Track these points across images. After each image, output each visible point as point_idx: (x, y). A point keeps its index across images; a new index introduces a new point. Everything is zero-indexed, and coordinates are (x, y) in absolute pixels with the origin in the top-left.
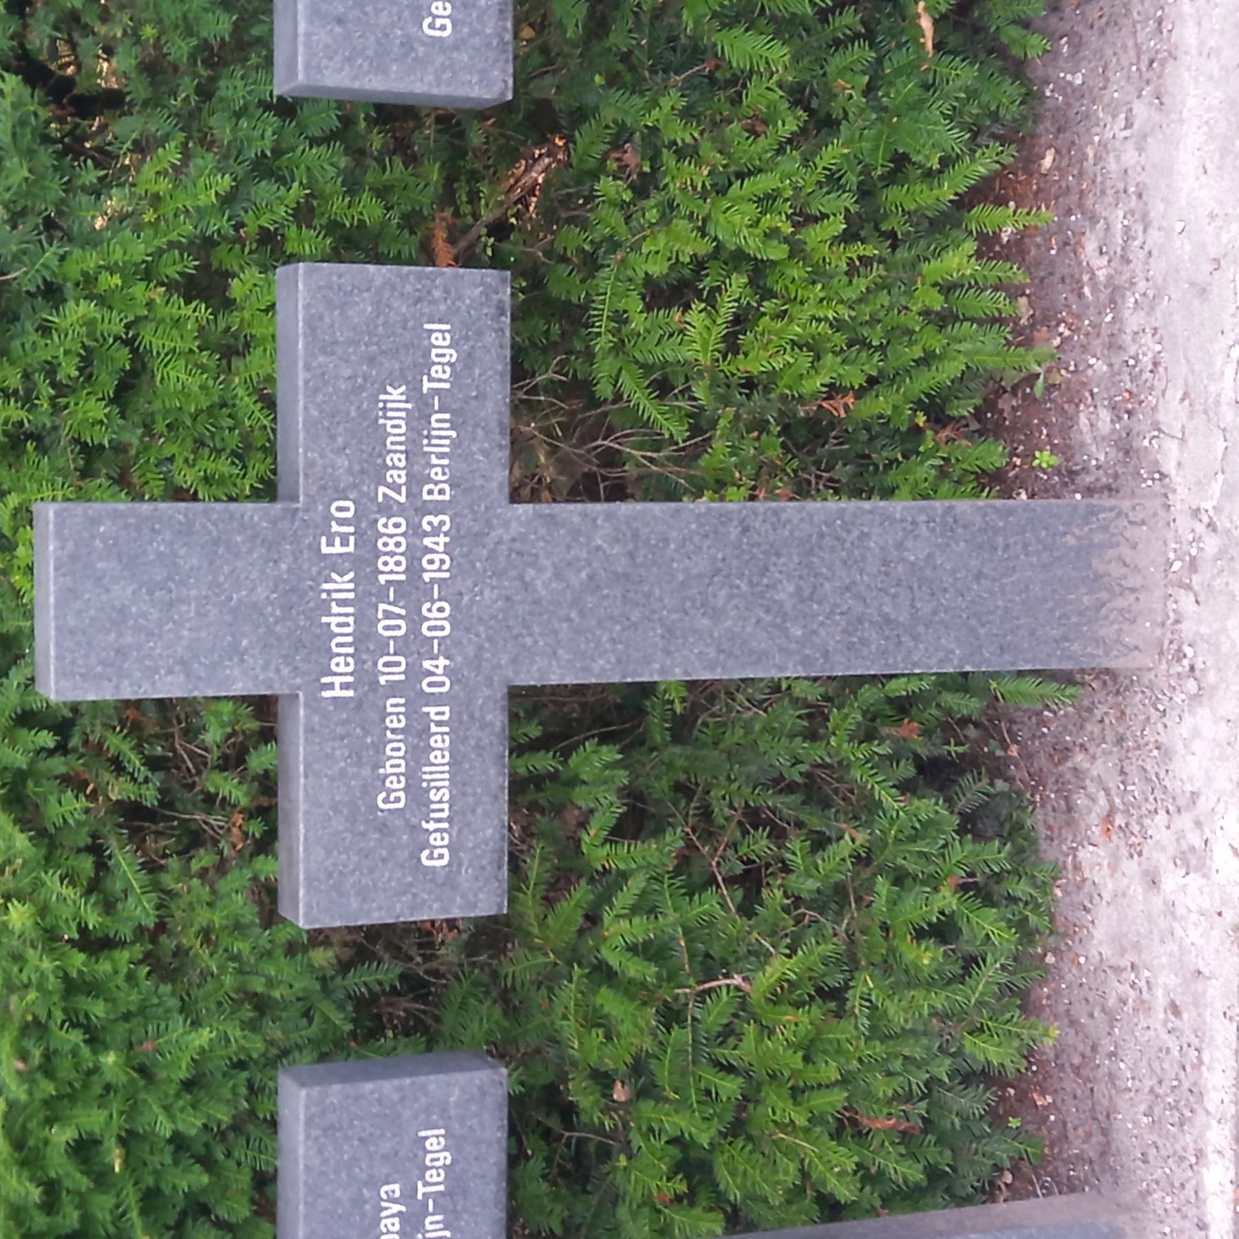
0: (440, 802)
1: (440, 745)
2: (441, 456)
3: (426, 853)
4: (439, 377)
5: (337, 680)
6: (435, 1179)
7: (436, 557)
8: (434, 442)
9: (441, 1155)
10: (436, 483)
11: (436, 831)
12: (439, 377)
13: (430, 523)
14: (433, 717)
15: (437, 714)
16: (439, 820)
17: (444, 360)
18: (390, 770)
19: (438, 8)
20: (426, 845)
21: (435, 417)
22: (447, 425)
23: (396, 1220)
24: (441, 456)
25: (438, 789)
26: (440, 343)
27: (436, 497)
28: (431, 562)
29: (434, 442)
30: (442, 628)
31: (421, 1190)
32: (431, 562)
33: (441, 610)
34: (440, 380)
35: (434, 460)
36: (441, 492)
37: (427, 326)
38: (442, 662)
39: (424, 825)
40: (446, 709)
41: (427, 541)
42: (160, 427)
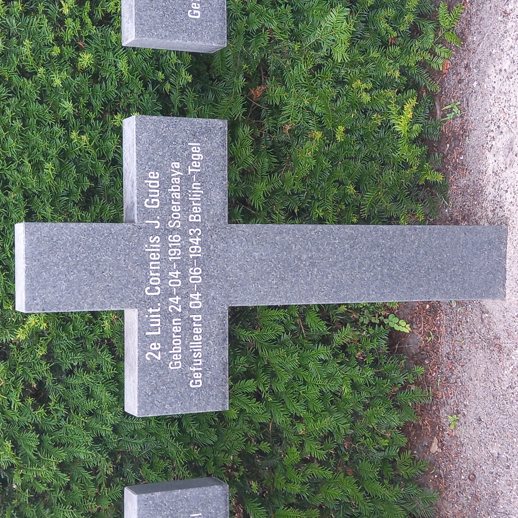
0: (198, 358)
1: (197, 332)
2: (196, 202)
4: (195, 167)
6: (196, 166)
7: (195, 247)
8: (194, 195)
9: (199, 155)
10: (194, 214)
11: (196, 371)
12: (195, 167)
13: (192, 232)
14: (194, 319)
17: (198, 159)
18: (174, 351)
19: (194, 6)
20: (191, 377)
23: (179, 179)
24: (196, 202)
25: (197, 352)
27: (195, 220)
28: (193, 249)
29: (194, 195)
30: (198, 279)
32: (193, 249)
34: (197, 168)
35: (194, 204)
37: (189, 144)
38: (198, 295)
40: (200, 316)
41: (191, 240)
42: (32, 121)
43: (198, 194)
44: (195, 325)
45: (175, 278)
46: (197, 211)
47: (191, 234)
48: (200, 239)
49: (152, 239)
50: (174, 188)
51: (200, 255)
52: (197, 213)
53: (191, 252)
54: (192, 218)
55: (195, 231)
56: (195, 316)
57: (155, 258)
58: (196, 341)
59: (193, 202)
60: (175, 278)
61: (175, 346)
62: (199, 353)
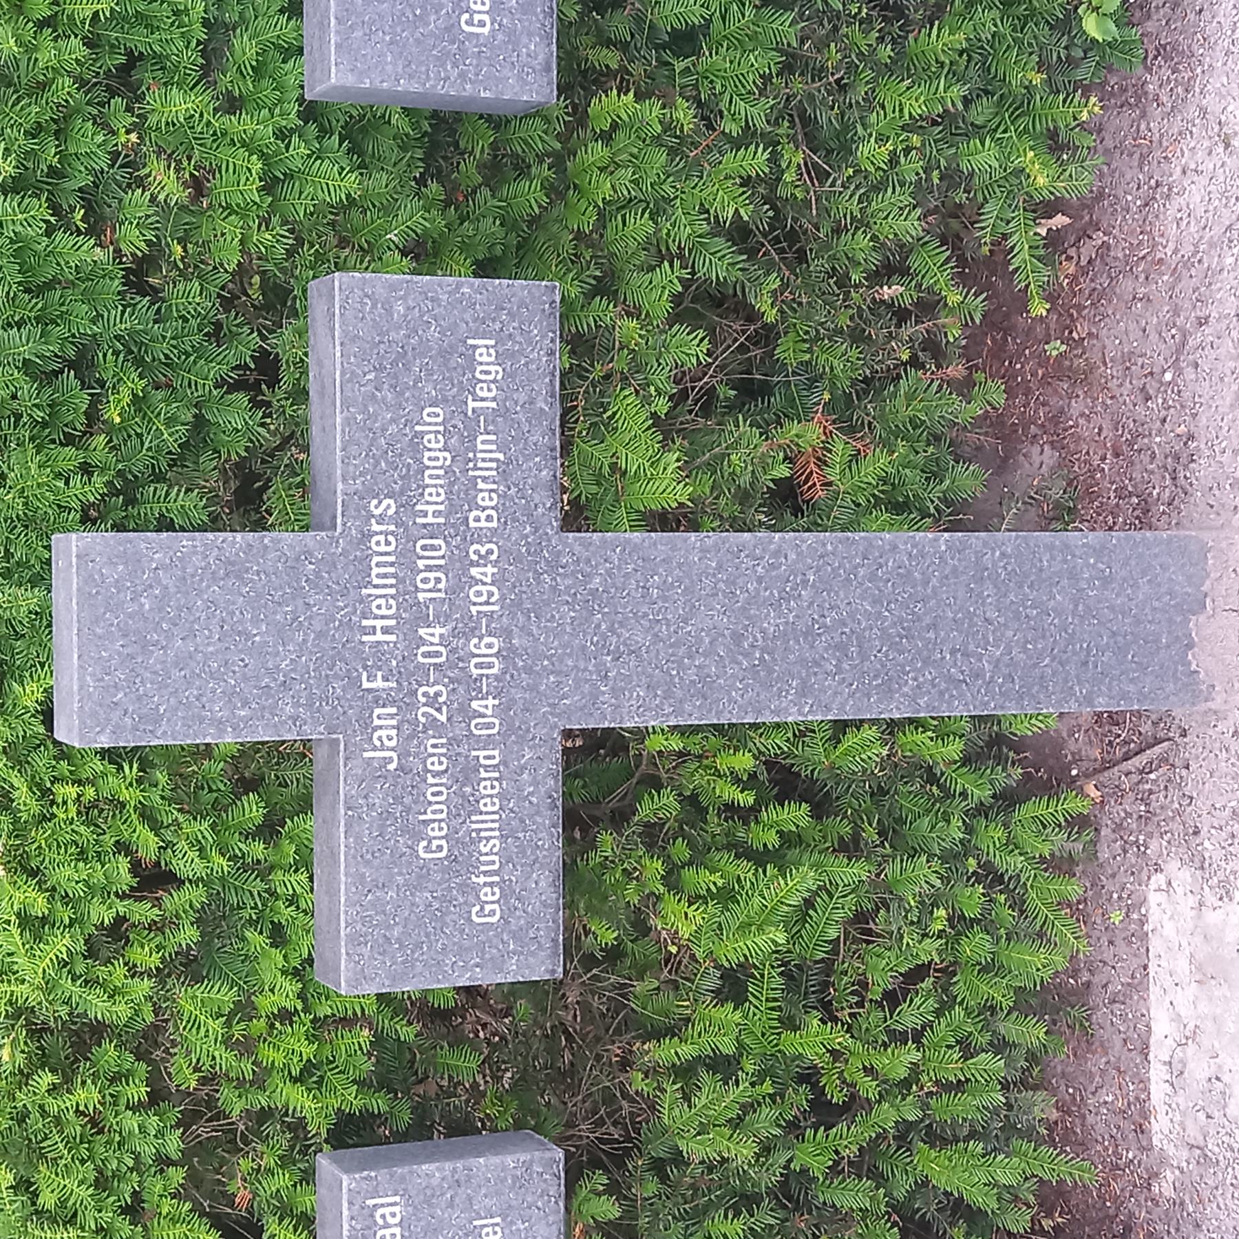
1: (489, 792)
3: (466, 16)
4: (485, 398)
5: (379, 623)
9: (492, 368)
11: (485, 884)
12: (485, 398)
13: (476, 552)
15: (486, 758)
16: (485, 873)
18: (430, 816)
21: (480, 438)
22: (494, 447)
25: (488, 839)
26: (485, 359)
27: (483, 524)
28: (479, 594)
29: (480, 465)
30: (490, 666)
31: (471, 404)
32: (479, 594)
33: (490, 646)
34: (483, 399)
35: (481, 485)
36: (489, 519)
39: (474, 879)
40: (496, 753)
41: (474, 571)
43: (491, 460)
44: (483, 774)
45: (432, 644)
46: (487, 503)
47: (475, 558)
48: (495, 570)
49: (376, 507)
50: (434, 812)
51: (496, 608)
52: (487, 508)
53: (474, 599)
54: (477, 520)
55: (483, 552)
56: (482, 754)
57: (383, 548)
58: (487, 813)
59: (479, 480)
60: (432, 644)
61: (428, 468)
62: (492, 842)
